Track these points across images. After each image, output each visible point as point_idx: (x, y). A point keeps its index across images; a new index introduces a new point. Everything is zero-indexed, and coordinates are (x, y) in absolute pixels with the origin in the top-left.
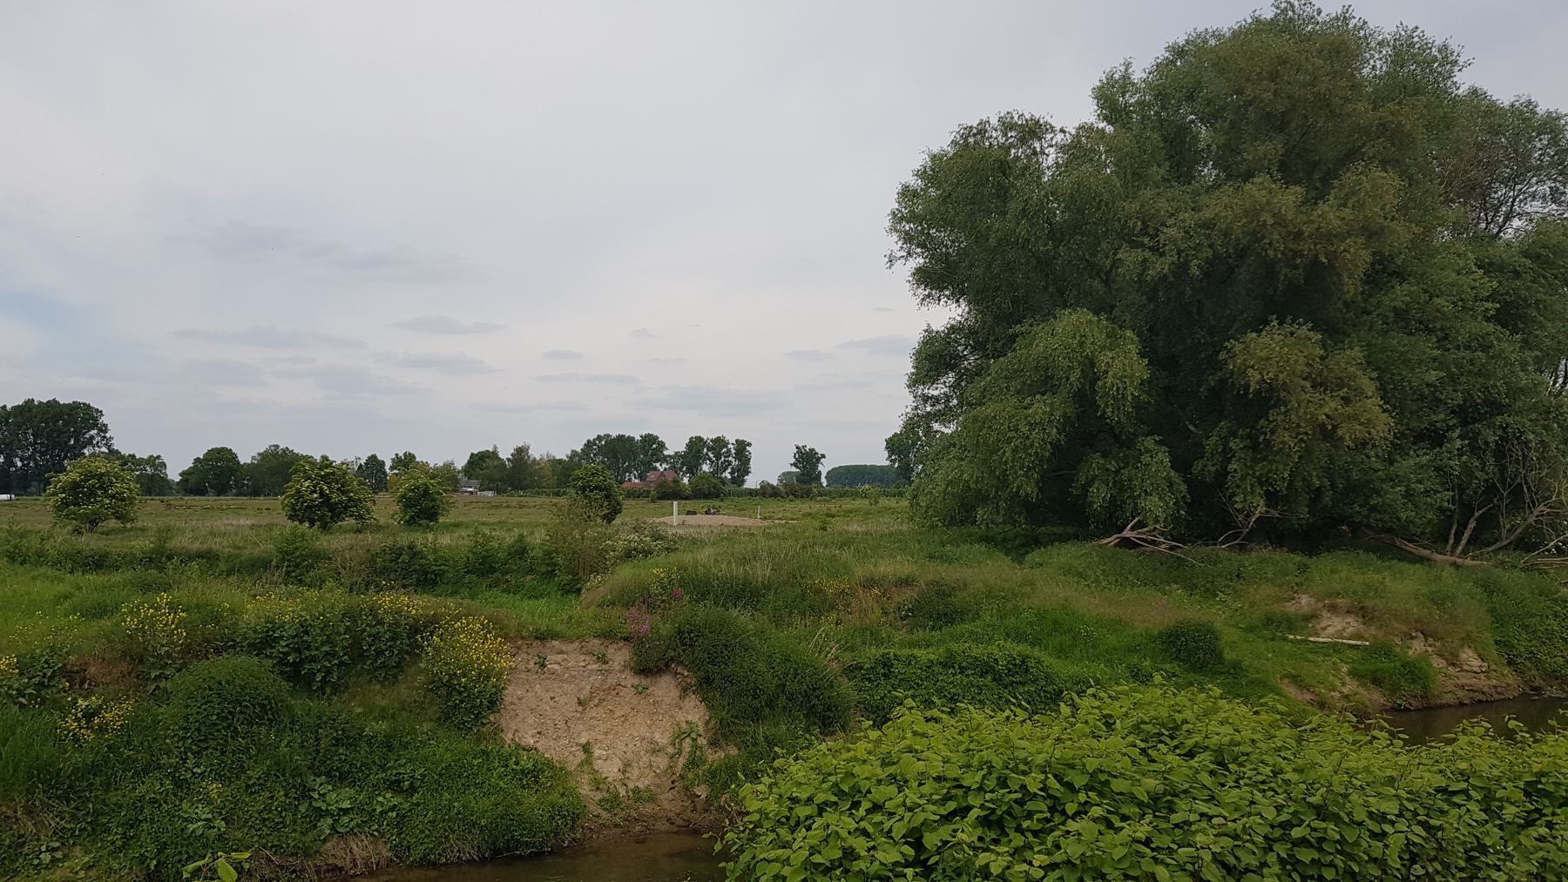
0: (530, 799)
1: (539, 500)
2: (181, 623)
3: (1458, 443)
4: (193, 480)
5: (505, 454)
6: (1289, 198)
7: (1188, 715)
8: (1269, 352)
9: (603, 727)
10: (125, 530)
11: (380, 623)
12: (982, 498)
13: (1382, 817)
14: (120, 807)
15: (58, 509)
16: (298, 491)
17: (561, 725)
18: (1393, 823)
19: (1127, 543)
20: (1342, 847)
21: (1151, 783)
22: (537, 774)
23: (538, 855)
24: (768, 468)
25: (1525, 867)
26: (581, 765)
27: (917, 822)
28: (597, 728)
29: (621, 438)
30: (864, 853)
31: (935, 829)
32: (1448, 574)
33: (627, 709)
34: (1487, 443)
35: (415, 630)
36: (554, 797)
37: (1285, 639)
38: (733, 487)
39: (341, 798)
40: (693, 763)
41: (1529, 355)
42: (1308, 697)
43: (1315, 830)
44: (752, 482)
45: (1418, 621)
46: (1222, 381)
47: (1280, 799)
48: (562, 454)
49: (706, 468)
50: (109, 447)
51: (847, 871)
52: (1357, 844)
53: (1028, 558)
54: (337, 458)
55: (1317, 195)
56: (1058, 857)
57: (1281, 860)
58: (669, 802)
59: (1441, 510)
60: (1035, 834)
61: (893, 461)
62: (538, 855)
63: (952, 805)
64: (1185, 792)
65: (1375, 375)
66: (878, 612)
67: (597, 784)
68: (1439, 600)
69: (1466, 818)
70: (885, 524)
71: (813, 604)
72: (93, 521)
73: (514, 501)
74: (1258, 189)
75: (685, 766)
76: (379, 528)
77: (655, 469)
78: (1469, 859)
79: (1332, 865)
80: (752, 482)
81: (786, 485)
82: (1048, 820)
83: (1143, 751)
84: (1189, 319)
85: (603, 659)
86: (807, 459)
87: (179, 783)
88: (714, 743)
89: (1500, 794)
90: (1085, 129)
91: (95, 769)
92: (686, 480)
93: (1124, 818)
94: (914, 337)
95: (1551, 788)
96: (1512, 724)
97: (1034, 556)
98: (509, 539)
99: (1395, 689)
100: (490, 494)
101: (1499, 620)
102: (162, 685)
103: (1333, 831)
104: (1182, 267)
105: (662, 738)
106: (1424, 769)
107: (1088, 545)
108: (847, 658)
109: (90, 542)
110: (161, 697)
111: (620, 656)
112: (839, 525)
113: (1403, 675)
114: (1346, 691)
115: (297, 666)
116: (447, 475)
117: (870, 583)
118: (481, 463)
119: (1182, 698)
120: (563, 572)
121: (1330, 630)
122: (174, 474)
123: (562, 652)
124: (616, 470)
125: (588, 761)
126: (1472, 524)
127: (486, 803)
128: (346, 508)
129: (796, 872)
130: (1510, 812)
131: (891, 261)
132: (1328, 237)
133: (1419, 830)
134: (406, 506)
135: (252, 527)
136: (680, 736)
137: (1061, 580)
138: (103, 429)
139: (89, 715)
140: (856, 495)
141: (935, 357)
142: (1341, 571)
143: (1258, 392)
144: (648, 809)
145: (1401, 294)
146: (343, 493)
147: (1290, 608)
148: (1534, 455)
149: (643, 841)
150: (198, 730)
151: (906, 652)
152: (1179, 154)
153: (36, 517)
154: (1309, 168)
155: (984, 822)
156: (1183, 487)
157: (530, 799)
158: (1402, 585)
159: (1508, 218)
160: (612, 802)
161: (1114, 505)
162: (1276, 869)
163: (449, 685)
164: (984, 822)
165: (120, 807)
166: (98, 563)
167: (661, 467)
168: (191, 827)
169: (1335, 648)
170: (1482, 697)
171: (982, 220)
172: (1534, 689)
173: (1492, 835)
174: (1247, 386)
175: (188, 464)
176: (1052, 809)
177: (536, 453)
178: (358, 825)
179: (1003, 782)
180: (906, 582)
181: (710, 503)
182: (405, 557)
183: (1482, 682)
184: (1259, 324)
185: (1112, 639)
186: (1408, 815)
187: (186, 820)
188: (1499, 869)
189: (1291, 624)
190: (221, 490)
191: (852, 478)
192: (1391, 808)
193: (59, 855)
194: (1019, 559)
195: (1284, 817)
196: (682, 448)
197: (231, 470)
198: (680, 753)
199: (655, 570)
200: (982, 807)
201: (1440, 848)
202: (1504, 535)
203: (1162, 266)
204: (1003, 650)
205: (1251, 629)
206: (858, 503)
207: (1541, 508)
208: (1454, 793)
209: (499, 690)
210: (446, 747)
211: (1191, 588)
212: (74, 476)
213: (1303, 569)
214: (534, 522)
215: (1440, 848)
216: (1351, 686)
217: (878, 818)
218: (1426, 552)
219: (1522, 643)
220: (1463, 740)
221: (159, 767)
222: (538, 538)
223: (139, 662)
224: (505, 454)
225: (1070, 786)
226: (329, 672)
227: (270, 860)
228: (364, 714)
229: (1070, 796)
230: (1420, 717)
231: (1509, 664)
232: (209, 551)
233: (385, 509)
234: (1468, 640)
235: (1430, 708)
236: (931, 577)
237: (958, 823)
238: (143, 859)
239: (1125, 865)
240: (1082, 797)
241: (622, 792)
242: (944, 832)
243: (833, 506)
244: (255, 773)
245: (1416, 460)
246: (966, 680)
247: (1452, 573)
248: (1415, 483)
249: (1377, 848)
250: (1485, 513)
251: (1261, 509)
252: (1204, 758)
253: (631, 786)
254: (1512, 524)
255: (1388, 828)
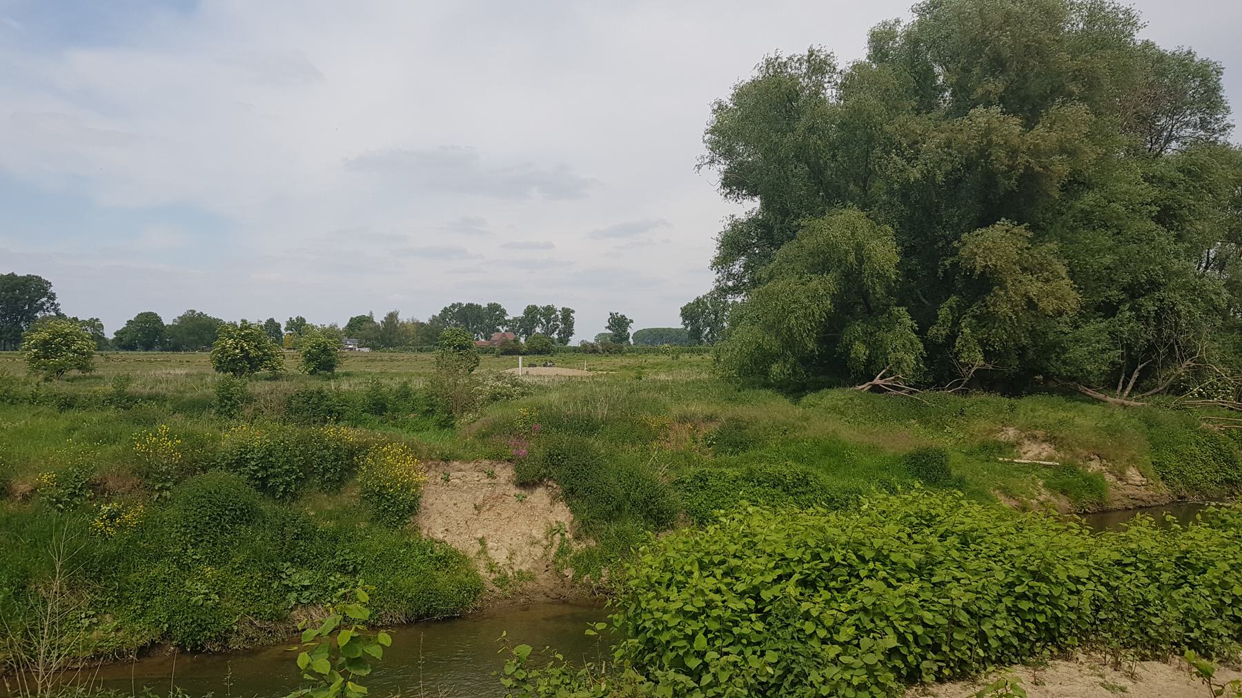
0: (442, 578)
1: (406, 355)
2: (179, 448)
3: (1128, 313)
4: (126, 338)
5: (379, 318)
6: (1014, 125)
7: (940, 511)
8: (994, 244)
9: (493, 526)
10: (86, 378)
11: (327, 448)
12: (774, 357)
13: (1077, 580)
14: (139, 584)
15: (32, 361)
16: (224, 348)
17: (463, 524)
18: (1084, 584)
19: (876, 389)
20: (1052, 601)
21: (919, 556)
22: (448, 559)
23: (451, 619)
24: (588, 329)
25: (1176, 614)
26: (479, 553)
27: (756, 582)
28: (494, 528)
29: (470, 306)
30: (720, 604)
31: (768, 588)
32: (1120, 415)
33: (511, 512)
34: (1149, 312)
35: (351, 454)
36: (461, 577)
37: (996, 461)
38: (559, 345)
39: (303, 577)
40: (562, 552)
41: (1181, 247)
42: (1014, 503)
43: (1032, 587)
44: (574, 341)
45: (1096, 447)
46: (955, 265)
47: (1008, 567)
48: (425, 320)
49: (538, 330)
50: (56, 310)
51: (708, 616)
52: (1059, 597)
53: (804, 400)
54: (252, 320)
55: (1029, 125)
56: (855, 606)
57: (1008, 610)
58: (545, 580)
59: (1113, 363)
60: (838, 591)
61: (686, 326)
62: (451, 619)
63: (779, 572)
64: (940, 563)
65: (1066, 262)
66: (690, 441)
67: (491, 567)
68: (1112, 431)
69: (1136, 582)
70: (684, 375)
71: (643, 435)
72: (60, 371)
73: (386, 356)
74: (980, 116)
75: (556, 554)
76: (290, 378)
77: (498, 331)
78: (1137, 610)
79: (1043, 612)
80: (574, 341)
81: (602, 344)
82: (846, 582)
83: (909, 535)
84: (928, 220)
85: (491, 475)
86: (619, 323)
87: (182, 567)
88: (577, 538)
89: (1158, 565)
90: (858, 67)
91: (119, 557)
92: (522, 340)
93: (899, 580)
94: (720, 226)
95: (1193, 561)
96: (1169, 518)
97: (810, 398)
98: (395, 384)
99: (1078, 497)
100: (366, 350)
101: (1156, 447)
102: (164, 494)
103: (1044, 588)
104: (928, 177)
105: (538, 534)
106: (1106, 550)
107: (848, 389)
108: (674, 476)
109: (60, 387)
110: (164, 503)
111: (505, 473)
112: (650, 375)
113: (1084, 487)
114: (1041, 499)
115: (264, 480)
116: (331, 332)
117: (683, 419)
118: (358, 325)
119: (936, 499)
120: (441, 410)
121: (1030, 454)
122: (109, 335)
123: (460, 470)
124: (467, 330)
125: (483, 551)
126: (1136, 375)
127: (411, 581)
128: (262, 361)
129: (673, 617)
130: (1165, 577)
131: (699, 167)
132: (1035, 152)
133: (1102, 588)
134: (309, 360)
135: (187, 375)
136: (551, 532)
137: (829, 415)
138: (52, 297)
139: (112, 517)
140: (657, 352)
141: (734, 243)
142: (1039, 409)
143: (983, 273)
144: (530, 585)
145: (1088, 199)
146: (259, 349)
147: (1002, 437)
148: (1183, 322)
149: (527, 609)
150: (196, 527)
151: (716, 471)
152: (923, 90)
153: (12, 365)
154: (1026, 104)
155: (803, 583)
156: (921, 346)
157: (442, 578)
158: (1084, 419)
159: (1168, 140)
160: (503, 581)
161: (870, 361)
162: (1005, 614)
163: (379, 494)
164: (803, 583)
165: (139, 584)
166: (67, 404)
167: (503, 329)
168: (194, 599)
169: (1034, 467)
170: (1141, 503)
171: (779, 139)
172: (1180, 497)
173: (1152, 594)
174: (972, 270)
175: (122, 325)
176: (850, 575)
177: (403, 318)
178: (316, 598)
179: (816, 556)
180: (710, 418)
181: (543, 357)
182: (315, 399)
183: (1142, 493)
184: (986, 220)
185: (868, 461)
186: (1095, 579)
187: (190, 594)
188: (1156, 615)
189: (1001, 448)
190: (148, 347)
191: (655, 339)
192: (1083, 574)
193: (95, 620)
194: (797, 400)
195: (1010, 579)
196: (521, 314)
197: (156, 330)
198: (552, 544)
199: (519, 410)
200: (801, 573)
201: (1117, 602)
202: (1160, 383)
203: (915, 174)
204: (789, 469)
205: (970, 453)
206: (662, 358)
207: (1188, 362)
208: (1126, 565)
209: (417, 499)
210: (379, 539)
211: (925, 422)
212: (45, 335)
213: (1012, 408)
214: (414, 372)
215: (1117, 602)
216: (1045, 495)
217: (728, 580)
218: (1101, 396)
219: (1173, 462)
220: (1133, 529)
221: (167, 555)
222: (419, 384)
223: (148, 476)
224: (379, 318)
225: (863, 559)
226: (288, 484)
227: (252, 623)
228: (316, 516)
229: (862, 566)
230: (1100, 517)
231: (1163, 479)
232: (158, 394)
233: (291, 362)
234: (1132, 461)
235: (1104, 512)
236: (730, 414)
237: (783, 583)
238: (158, 623)
239: (902, 610)
240: (871, 565)
241: (510, 574)
242: (776, 590)
243: (641, 359)
244: (239, 559)
245: (1094, 327)
246: (762, 491)
247: (1121, 407)
248: (1091, 345)
249: (1074, 601)
250: (1143, 365)
251: (979, 361)
252: (953, 540)
253: (516, 569)
254: (1165, 377)
255: (1080, 587)
